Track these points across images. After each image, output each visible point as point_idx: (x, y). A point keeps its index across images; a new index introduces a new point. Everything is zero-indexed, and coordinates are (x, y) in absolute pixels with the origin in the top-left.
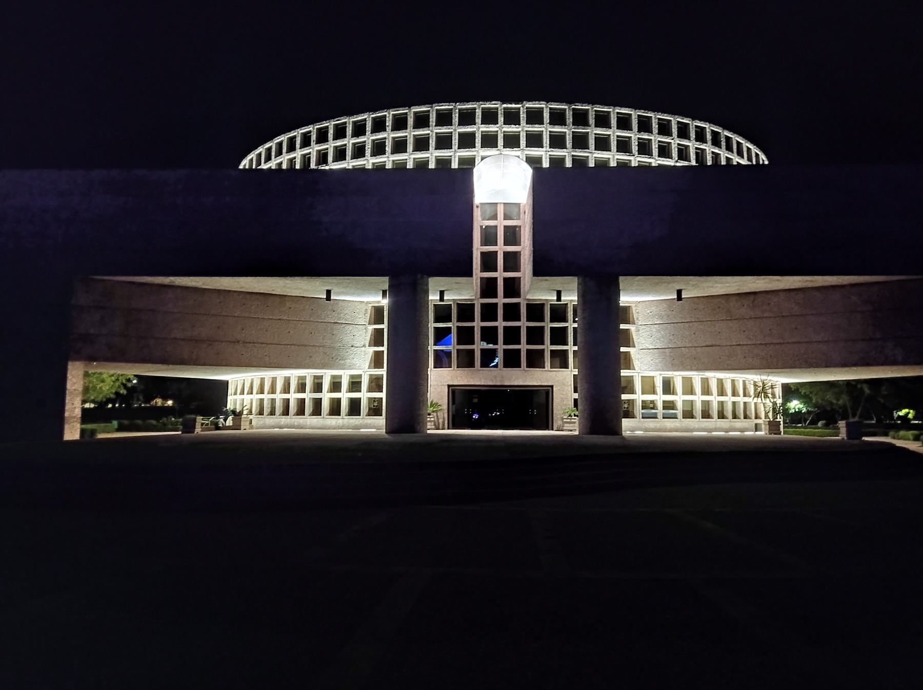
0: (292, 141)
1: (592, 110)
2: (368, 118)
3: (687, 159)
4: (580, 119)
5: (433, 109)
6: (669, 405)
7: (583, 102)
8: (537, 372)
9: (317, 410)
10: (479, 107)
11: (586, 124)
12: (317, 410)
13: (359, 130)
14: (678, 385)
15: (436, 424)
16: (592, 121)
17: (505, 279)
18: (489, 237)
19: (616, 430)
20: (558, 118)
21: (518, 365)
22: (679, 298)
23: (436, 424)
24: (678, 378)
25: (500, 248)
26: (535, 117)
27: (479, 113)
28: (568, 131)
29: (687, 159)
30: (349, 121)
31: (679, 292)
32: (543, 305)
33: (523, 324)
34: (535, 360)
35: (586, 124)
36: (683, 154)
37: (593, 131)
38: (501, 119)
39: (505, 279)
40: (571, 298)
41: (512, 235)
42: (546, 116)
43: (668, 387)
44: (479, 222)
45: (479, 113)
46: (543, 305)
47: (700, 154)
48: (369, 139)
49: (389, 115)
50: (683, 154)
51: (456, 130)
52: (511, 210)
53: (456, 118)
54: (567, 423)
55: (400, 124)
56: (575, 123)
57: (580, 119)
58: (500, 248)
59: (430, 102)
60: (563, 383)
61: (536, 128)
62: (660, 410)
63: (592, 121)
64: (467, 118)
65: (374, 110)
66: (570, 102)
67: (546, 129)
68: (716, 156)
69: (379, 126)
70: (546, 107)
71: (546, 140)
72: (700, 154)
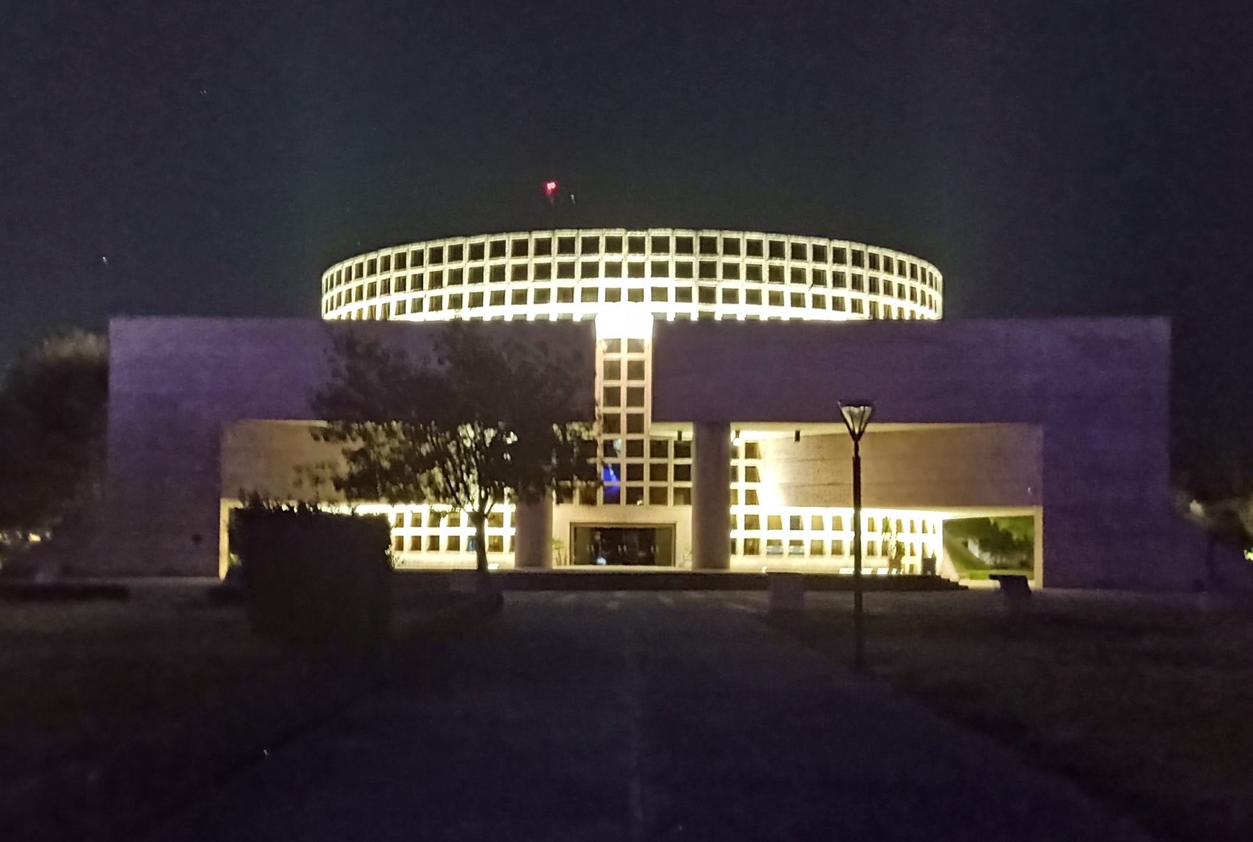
0: (386, 261)
1: (720, 236)
2: (486, 240)
3: (861, 311)
4: (708, 246)
5: (555, 236)
6: (797, 543)
7: (710, 228)
8: (659, 509)
9: (434, 544)
10: (602, 235)
11: (713, 251)
12: (434, 544)
13: (477, 253)
14: (806, 522)
15: (560, 558)
16: (720, 248)
17: (629, 416)
18: (612, 371)
19: (725, 565)
20: (684, 246)
21: (618, 501)
22: (798, 438)
23: (560, 558)
24: (807, 514)
25: (624, 383)
26: (660, 245)
27: (602, 243)
28: (695, 259)
29: (861, 311)
30: (466, 243)
31: (798, 434)
32: (667, 442)
33: (646, 461)
34: (658, 497)
35: (713, 251)
36: (856, 306)
37: (721, 259)
38: (625, 248)
39: (629, 416)
40: (689, 434)
41: (636, 370)
42: (672, 245)
43: (796, 524)
44: (601, 357)
45: (602, 243)
46: (667, 442)
47: (873, 306)
48: (487, 263)
49: (509, 239)
50: (856, 306)
51: (579, 259)
52: (635, 346)
53: (578, 246)
54: (684, 560)
55: (520, 249)
56: (702, 251)
57: (708, 246)
58: (624, 383)
59: (553, 228)
60: (681, 518)
61: (661, 258)
62: (786, 548)
63: (720, 248)
64: (590, 246)
65: (493, 233)
66: (697, 228)
67: (672, 259)
68: (901, 311)
69: (498, 250)
70: (672, 235)
71: (672, 269)
72: (873, 306)
